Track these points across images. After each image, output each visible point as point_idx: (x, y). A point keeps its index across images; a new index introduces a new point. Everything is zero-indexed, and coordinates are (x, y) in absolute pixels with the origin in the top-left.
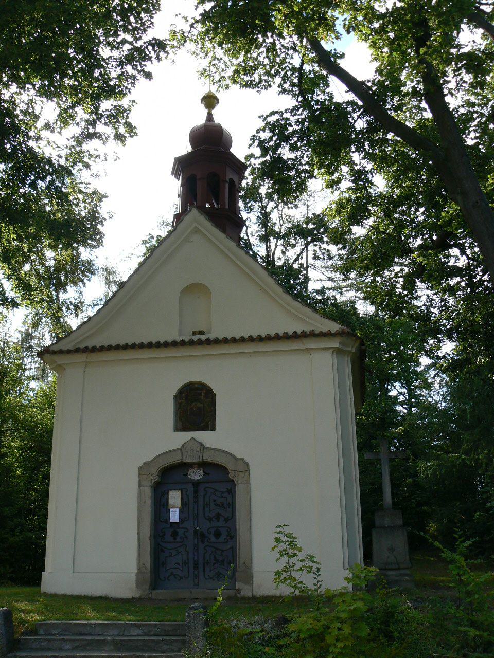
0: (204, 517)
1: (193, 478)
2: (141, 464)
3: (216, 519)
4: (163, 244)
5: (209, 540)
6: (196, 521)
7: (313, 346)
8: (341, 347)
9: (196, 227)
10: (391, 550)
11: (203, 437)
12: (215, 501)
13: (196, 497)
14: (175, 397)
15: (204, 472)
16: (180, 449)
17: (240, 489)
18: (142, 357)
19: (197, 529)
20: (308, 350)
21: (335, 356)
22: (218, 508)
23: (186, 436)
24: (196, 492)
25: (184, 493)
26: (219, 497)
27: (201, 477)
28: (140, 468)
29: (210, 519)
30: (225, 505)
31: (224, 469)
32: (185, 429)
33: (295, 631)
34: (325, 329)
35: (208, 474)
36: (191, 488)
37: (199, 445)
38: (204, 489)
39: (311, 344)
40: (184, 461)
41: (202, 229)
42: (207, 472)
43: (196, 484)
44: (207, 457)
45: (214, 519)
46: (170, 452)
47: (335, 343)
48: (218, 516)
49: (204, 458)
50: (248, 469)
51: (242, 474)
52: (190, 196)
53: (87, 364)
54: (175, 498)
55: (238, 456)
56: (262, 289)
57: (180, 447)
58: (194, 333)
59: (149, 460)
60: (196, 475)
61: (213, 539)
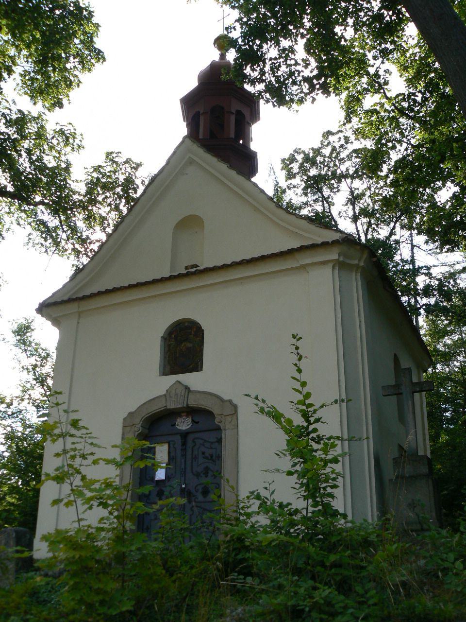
0: (192, 472)
1: (181, 428)
2: (125, 415)
3: (204, 474)
4: (156, 180)
5: (196, 500)
6: (183, 478)
7: (308, 261)
8: (341, 259)
9: (190, 157)
10: (412, 506)
11: (190, 379)
12: (203, 453)
13: (184, 450)
14: (164, 339)
15: (193, 420)
16: (165, 395)
17: (227, 436)
18: (131, 298)
19: (183, 486)
20: (304, 267)
21: (336, 271)
22: (207, 461)
23: (172, 379)
24: (184, 444)
25: (171, 445)
26: (207, 448)
27: (189, 426)
28: (125, 419)
29: (198, 475)
30: (214, 458)
31: (209, 414)
32: (173, 372)
33: (98, 481)
34: (319, 241)
35: (197, 423)
36: (178, 439)
37: (183, 388)
38: (193, 440)
39: (306, 259)
40: (168, 407)
41: (195, 158)
42: (197, 421)
43: (185, 435)
44: (193, 402)
45: (202, 475)
46: (154, 399)
47: (333, 255)
48: (206, 471)
49: (189, 403)
50: (236, 411)
51: (229, 419)
52: (194, 134)
53: (80, 314)
54: (162, 452)
55: (226, 398)
56: (256, 209)
57: (165, 392)
58: (186, 268)
59: (133, 410)
60: (184, 424)
61: (200, 498)
